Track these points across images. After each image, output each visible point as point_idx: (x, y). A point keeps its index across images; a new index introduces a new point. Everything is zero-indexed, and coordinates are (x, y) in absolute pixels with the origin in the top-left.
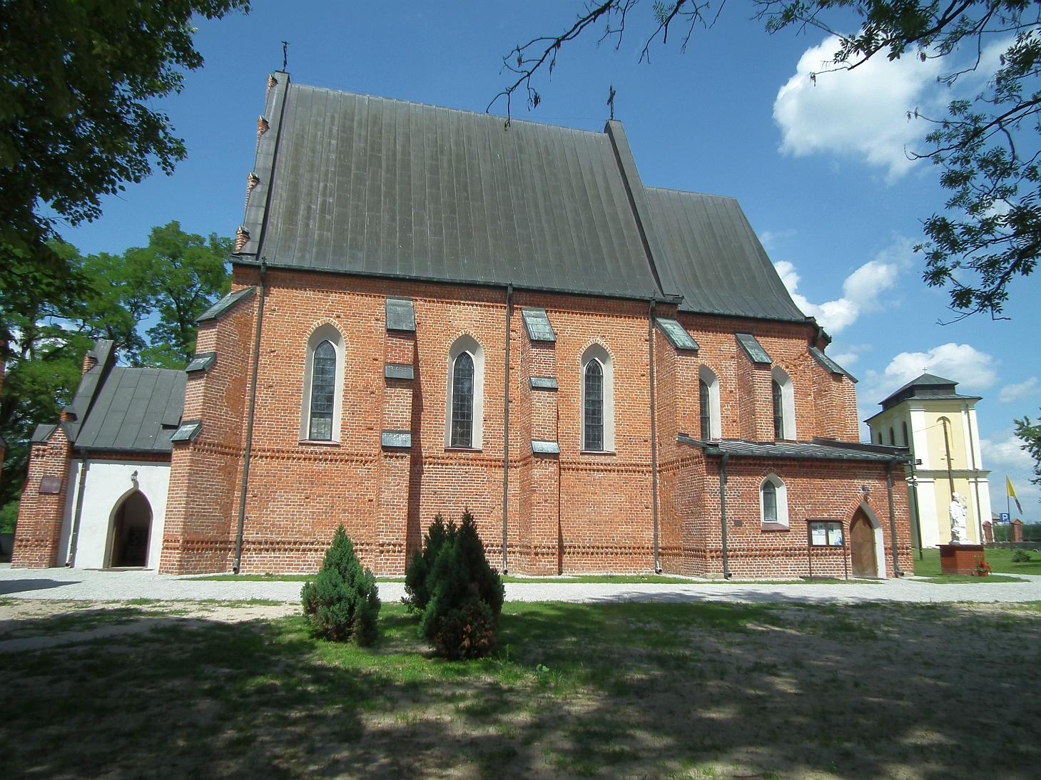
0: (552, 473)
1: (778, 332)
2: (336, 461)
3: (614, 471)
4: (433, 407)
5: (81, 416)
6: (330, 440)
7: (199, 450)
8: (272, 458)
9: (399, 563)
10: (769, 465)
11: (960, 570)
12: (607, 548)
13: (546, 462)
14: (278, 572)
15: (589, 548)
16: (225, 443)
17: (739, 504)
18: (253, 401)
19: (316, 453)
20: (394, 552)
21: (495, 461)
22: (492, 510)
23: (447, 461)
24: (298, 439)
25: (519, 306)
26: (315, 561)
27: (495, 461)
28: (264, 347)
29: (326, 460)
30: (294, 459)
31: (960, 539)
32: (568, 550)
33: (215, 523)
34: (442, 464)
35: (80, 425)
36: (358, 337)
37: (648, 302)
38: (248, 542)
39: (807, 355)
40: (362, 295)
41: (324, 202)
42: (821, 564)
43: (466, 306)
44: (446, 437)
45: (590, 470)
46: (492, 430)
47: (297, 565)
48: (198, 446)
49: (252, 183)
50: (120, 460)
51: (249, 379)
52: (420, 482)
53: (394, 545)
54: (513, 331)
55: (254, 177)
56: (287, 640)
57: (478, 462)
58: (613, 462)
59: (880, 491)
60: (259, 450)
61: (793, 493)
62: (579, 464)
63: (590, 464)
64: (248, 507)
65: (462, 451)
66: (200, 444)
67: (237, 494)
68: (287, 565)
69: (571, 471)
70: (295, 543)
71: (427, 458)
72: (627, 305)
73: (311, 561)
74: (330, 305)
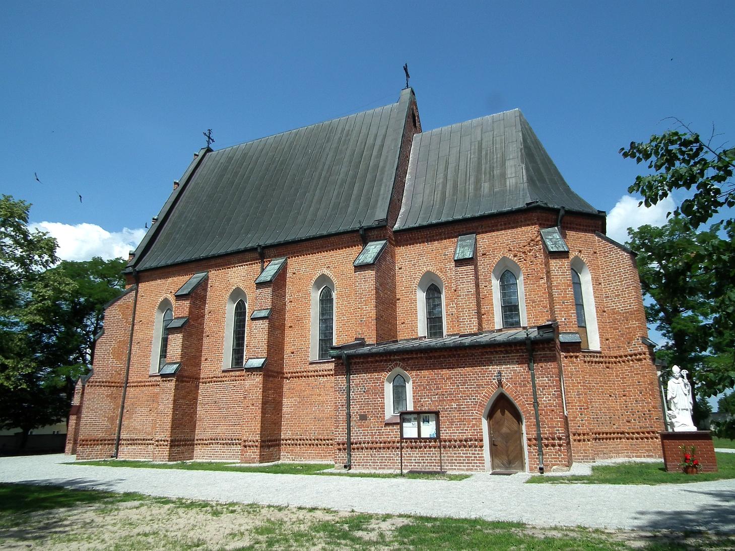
1: (505, 224)
10: (395, 360)
13: (254, 375)
14: (135, 458)
16: (113, 380)
17: (365, 399)
23: (223, 379)
33: (104, 428)
37: (357, 231)
42: (448, 457)
44: (227, 361)
45: (317, 376)
59: (522, 375)
61: (419, 386)
63: (317, 371)
72: (345, 238)
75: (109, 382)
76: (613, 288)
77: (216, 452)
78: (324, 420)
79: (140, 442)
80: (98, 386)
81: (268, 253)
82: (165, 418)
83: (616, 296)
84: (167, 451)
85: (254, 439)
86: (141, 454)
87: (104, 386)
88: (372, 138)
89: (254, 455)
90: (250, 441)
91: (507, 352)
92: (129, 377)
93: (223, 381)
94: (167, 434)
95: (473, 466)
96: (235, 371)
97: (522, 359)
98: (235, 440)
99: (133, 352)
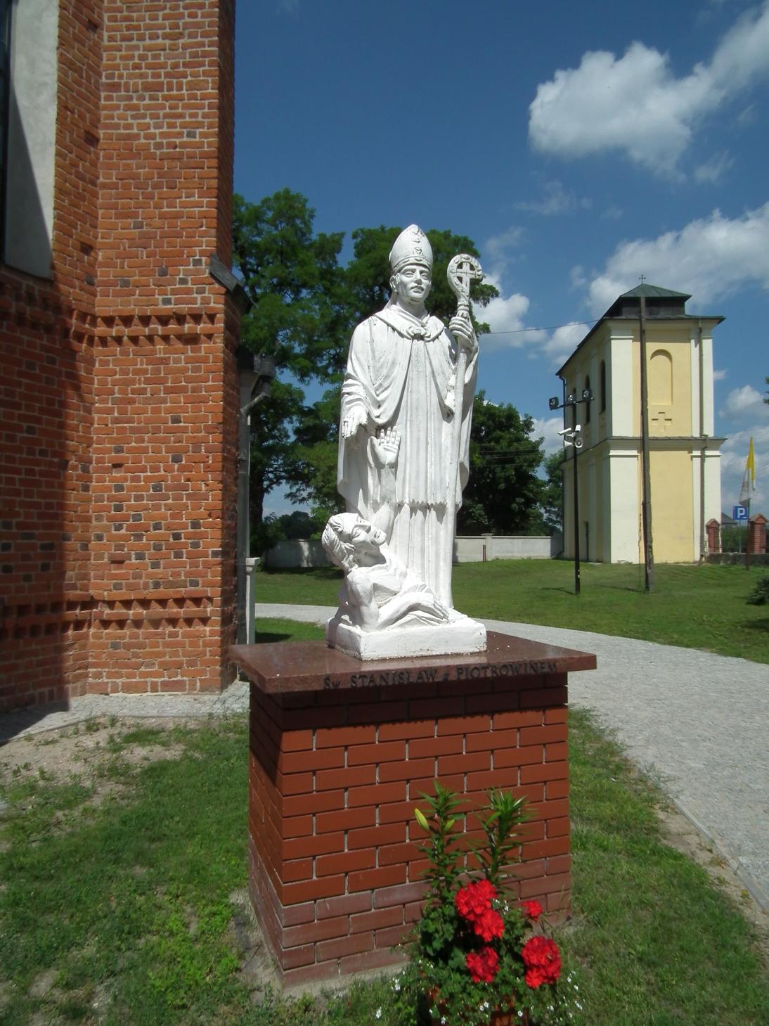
76: (142, 58)
83: (147, 87)
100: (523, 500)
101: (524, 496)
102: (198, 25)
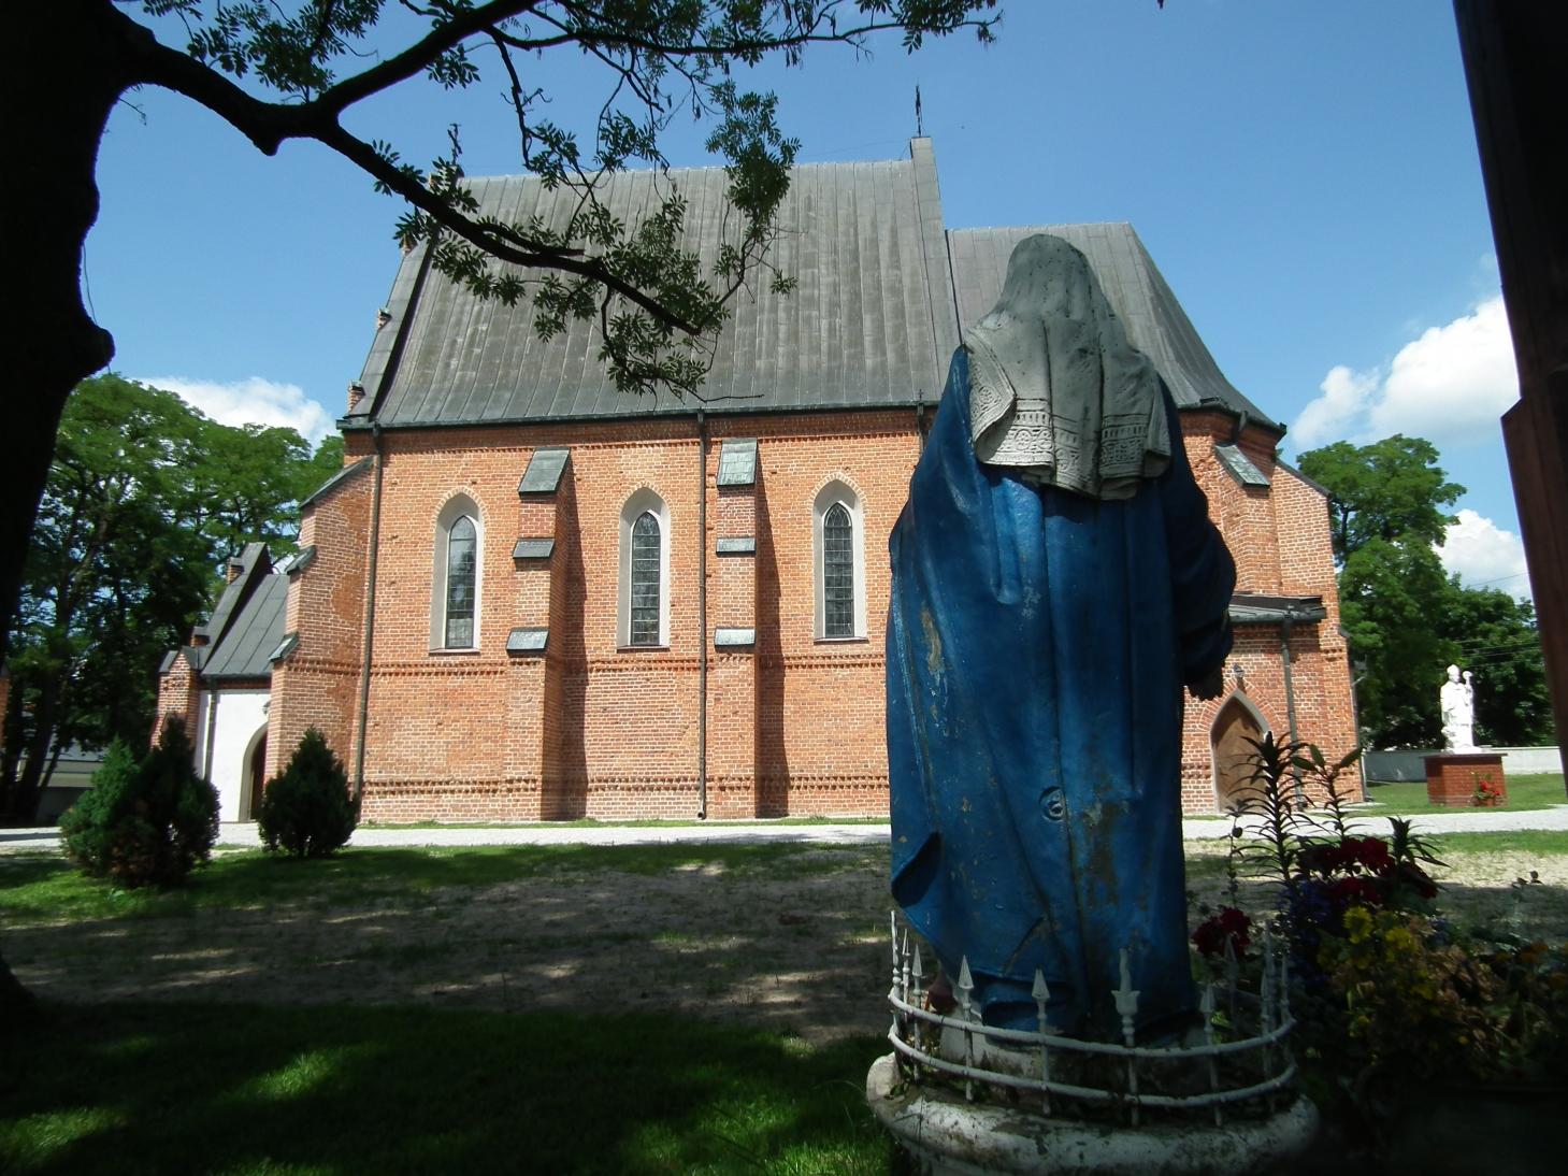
0: (744, 672)
2: (475, 673)
3: (867, 665)
4: (600, 592)
5: (213, 640)
6: (471, 647)
7: (296, 669)
8: (397, 674)
9: (533, 805)
11: (1449, 798)
12: (856, 778)
13: (735, 658)
14: (406, 820)
15: (828, 778)
18: (372, 604)
19: (451, 666)
20: (526, 790)
21: (688, 661)
22: (683, 729)
23: (621, 666)
24: (428, 648)
25: (719, 439)
26: (451, 805)
27: (688, 661)
28: (384, 533)
29: (462, 673)
30: (423, 674)
31: (1455, 745)
32: (796, 783)
34: (614, 670)
35: (210, 650)
36: (499, 507)
37: (913, 408)
38: (371, 784)
39: (1212, 459)
40: (504, 450)
41: (475, 331)
43: (644, 448)
44: (817, 624)
45: (829, 666)
46: (684, 618)
47: (429, 811)
48: (295, 665)
49: (380, 322)
50: (253, 688)
51: (367, 576)
52: (584, 696)
53: (527, 781)
54: (710, 475)
55: (383, 314)
56: (169, 894)
57: (664, 664)
58: (865, 652)
59: (1270, 671)
60: (381, 666)
62: (812, 658)
63: (829, 658)
64: (368, 740)
65: (641, 651)
66: (298, 661)
67: (356, 723)
68: (417, 811)
69: (800, 669)
70: (427, 783)
71: (593, 663)
72: (882, 417)
73: (447, 806)
74: (463, 469)
75: (330, 663)
76: (1297, 549)
77: (613, 804)
78: (848, 745)
79: (416, 788)
80: (308, 670)
81: (713, 427)
82: (526, 737)
83: (1301, 560)
84: (535, 800)
85: (743, 775)
86: (422, 811)
87: (321, 671)
88: (868, 227)
89: (743, 804)
90: (734, 779)
91: (1247, 637)
92: (374, 654)
93: (621, 670)
94: (534, 768)
95: (1196, 805)
96: (637, 651)
97: (1271, 647)
98: (656, 780)
99: (379, 602)
100: (1530, 704)
101: (1532, 699)
102: (1321, 534)
